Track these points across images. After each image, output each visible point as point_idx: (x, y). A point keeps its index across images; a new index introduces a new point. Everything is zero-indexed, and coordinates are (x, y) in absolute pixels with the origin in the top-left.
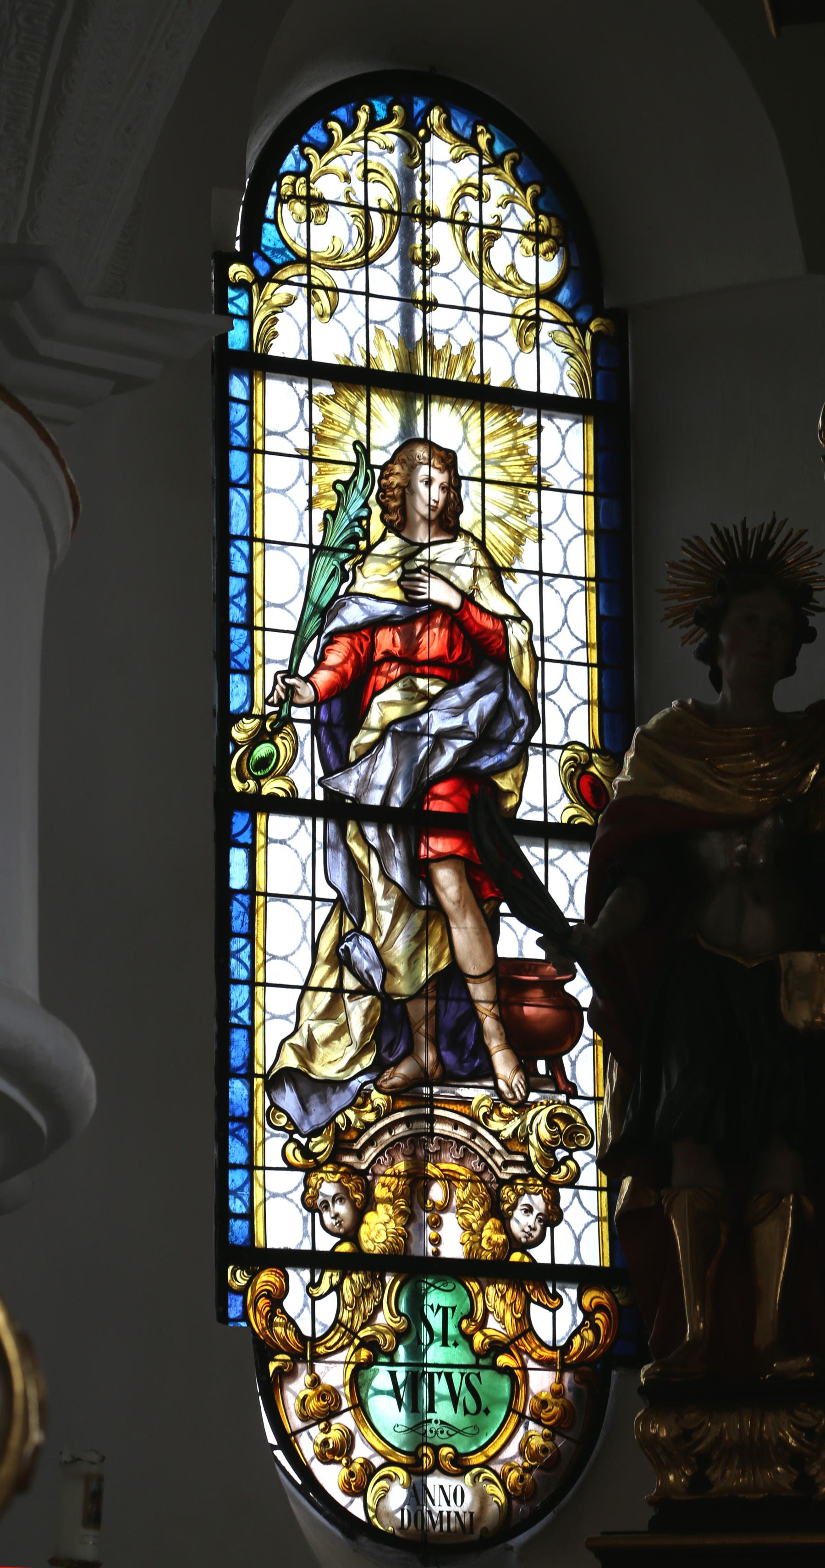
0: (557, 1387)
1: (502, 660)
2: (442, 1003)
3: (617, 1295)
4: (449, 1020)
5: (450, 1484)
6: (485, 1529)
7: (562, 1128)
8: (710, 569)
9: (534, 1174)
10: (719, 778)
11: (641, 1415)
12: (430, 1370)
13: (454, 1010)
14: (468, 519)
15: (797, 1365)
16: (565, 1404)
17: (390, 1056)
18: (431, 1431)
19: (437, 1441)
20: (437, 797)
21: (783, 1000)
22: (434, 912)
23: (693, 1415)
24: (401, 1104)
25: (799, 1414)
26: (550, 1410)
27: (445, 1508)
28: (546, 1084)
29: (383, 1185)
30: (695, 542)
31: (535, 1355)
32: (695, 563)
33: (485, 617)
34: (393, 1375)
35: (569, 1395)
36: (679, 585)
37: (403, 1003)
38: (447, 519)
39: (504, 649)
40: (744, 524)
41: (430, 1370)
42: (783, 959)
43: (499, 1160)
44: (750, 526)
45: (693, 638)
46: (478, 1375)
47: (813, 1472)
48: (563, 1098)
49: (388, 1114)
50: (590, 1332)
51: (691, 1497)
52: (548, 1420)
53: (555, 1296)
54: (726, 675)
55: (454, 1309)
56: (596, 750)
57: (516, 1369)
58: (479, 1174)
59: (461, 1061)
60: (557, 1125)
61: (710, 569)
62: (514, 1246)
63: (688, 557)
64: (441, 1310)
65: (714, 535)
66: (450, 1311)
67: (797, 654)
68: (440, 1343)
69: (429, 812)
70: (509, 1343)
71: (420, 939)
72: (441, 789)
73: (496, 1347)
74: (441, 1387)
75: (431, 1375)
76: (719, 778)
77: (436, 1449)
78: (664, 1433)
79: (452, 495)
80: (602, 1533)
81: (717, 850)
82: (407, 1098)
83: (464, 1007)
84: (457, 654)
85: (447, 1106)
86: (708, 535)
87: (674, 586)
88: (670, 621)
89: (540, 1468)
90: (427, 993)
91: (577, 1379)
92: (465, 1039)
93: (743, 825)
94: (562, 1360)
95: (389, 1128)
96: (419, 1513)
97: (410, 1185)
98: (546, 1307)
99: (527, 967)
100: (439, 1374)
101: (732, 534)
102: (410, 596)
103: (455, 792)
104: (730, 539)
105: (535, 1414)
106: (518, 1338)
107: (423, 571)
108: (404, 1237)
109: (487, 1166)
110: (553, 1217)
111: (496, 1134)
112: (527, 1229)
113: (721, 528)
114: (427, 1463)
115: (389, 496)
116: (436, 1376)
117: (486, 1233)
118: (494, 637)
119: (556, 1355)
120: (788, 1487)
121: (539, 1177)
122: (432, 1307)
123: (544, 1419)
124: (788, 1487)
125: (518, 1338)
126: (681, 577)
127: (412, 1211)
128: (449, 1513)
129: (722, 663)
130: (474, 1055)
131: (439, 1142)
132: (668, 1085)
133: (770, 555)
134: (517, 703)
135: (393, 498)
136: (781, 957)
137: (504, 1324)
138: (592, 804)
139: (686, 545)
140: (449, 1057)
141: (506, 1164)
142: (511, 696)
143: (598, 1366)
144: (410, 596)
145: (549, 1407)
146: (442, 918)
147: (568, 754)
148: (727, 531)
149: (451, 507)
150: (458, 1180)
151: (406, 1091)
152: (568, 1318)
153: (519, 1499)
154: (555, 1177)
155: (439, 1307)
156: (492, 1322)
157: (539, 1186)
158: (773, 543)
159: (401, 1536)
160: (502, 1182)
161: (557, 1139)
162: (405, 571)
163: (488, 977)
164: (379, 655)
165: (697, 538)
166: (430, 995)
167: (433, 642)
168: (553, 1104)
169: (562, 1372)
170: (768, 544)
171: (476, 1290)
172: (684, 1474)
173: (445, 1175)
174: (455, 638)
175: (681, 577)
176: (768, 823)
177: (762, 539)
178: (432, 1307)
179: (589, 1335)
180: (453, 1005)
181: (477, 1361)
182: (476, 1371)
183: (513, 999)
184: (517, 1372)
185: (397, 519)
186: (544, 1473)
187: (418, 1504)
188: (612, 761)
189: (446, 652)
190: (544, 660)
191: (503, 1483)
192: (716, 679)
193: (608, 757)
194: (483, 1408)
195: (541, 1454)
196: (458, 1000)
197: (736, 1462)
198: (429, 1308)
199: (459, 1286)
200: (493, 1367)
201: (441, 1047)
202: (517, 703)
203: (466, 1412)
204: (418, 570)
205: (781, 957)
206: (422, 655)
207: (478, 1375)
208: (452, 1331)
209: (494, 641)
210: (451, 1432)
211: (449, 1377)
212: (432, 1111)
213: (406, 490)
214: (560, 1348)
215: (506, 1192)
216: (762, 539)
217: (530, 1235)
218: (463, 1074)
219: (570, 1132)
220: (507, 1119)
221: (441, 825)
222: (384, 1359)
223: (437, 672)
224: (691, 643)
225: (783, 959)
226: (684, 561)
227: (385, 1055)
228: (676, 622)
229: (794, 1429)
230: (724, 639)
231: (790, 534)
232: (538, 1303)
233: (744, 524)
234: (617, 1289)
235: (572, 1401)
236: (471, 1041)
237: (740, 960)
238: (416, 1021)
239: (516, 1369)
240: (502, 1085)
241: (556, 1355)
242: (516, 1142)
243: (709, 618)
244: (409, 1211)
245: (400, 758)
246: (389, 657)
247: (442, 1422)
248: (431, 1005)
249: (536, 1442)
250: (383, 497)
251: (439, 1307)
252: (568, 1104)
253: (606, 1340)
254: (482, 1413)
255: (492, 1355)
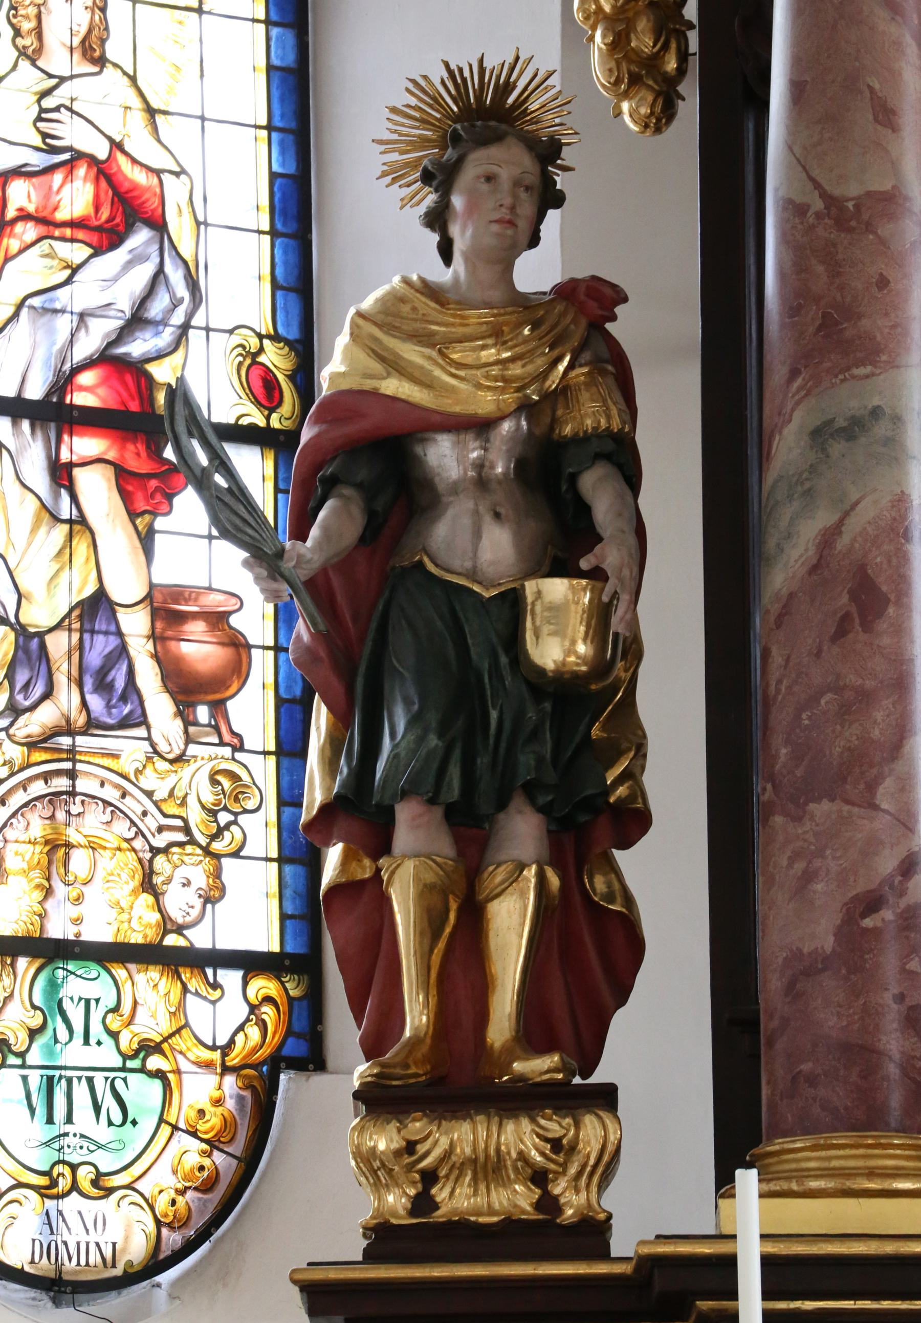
0: (217, 1094)
1: (159, 225)
2: (87, 636)
3: (287, 985)
4: (94, 659)
5: (91, 1208)
6: (130, 1263)
7: (226, 788)
8: (438, 116)
9: (193, 842)
10: (453, 370)
11: (357, 1124)
12: (69, 1073)
13: (100, 648)
14: (116, 49)
15: (539, 1066)
16: (226, 1114)
17: (25, 700)
18: (69, 1146)
19: (74, 1159)
20: (82, 388)
21: (529, 636)
22: (77, 527)
23: (418, 1124)
24: (37, 756)
25: (543, 1122)
26: (208, 1121)
27: (83, 1238)
28: (207, 734)
29: (16, 854)
30: (423, 83)
31: (189, 1055)
32: (420, 108)
33: (137, 169)
34: (25, 1078)
35: (230, 1104)
36: (400, 135)
37: (41, 635)
38: (91, 47)
39: (160, 210)
40: (481, 61)
41: (69, 1073)
42: (530, 587)
43: (154, 826)
44: (488, 65)
45: (413, 201)
46: (125, 1080)
47: (557, 1191)
48: (227, 751)
49: (22, 769)
50: (256, 1028)
51: (414, 1221)
52: (206, 1133)
53: (215, 986)
54: (459, 247)
55: (97, 1001)
56: (269, 337)
57: (170, 1072)
58: (128, 841)
59: (109, 706)
60: (219, 783)
61: (438, 116)
62: (169, 927)
63: (413, 101)
64: (83, 1001)
65: (445, 75)
66: (93, 1003)
67: (541, 223)
68: (82, 1041)
69: (72, 406)
70: (162, 1042)
71: (67, 550)
72: (87, 378)
73: (148, 1048)
74: (81, 1092)
75: (69, 1081)
76: (453, 370)
77: (74, 1168)
78: (382, 1146)
79: (97, 18)
80: (309, 1264)
81: (445, 457)
82: (46, 749)
83: (113, 642)
84: (105, 214)
85: (92, 760)
86: (438, 74)
87: (395, 137)
88: (388, 179)
89: (196, 1189)
90: (70, 624)
91: (240, 1084)
92: (113, 680)
93: (482, 427)
94: (223, 1062)
95: (24, 785)
96: (53, 1244)
97: (48, 853)
98: (205, 998)
99: (187, 595)
100: (79, 1079)
101: (467, 74)
102: (48, 141)
103: (104, 381)
104: (464, 80)
105: (190, 1126)
106: (172, 1035)
107: (62, 109)
108: (40, 915)
109: (140, 833)
110: (213, 896)
111: (149, 794)
112: (186, 908)
113: (453, 66)
114: (64, 1184)
115: (22, 16)
116: (75, 1081)
117: (135, 913)
118: (146, 196)
119: (216, 1056)
120: (528, 1208)
121: (200, 846)
122: (72, 999)
123: (200, 1132)
124: (528, 1208)
125: (172, 1035)
126: (403, 125)
127: (50, 885)
128: (88, 1244)
129: (455, 230)
130: (124, 698)
131: (83, 802)
132: (393, 735)
133: (510, 101)
134: (175, 275)
135: (27, 17)
136: (527, 584)
137: (156, 1019)
138: (263, 402)
139: (411, 86)
140: (96, 703)
141: (160, 829)
142: (169, 268)
143: (265, 1069)
144: (48, 141)
145: (207, 1117)
146: (88, 534)
147: (236, 339)
148: (461, 70)
149: (96, 32)
150: (105, 848)
151: (45, 740)
152: (233, 1009)
153: (170, 1226)
154: (216, 846)
155: (80, 999)
156: (142, 1015)
157: (198, 855)
158: (514, 87)
159: (32, 1271)
160: (155, 851)
161: (220, 800)
162: (42, 110)
163: (141, 606)
164: (11, 213)
165: (425, 77)
166: (73, 626)
167: (77, 197)
168: (216, 758)
169: (222, 1075)
170: (506, 88)
171: (123, 979)
172: (405, 1192)
173: (89, 842)
174: (102, 195)
175: (403, 125)
176: (506, 426)
177: (501, 81)
178: (72, 999)
179: (254, 1033)
180: (100, 639)
181: (124, 1063)
182: (123, 1075)
183: (169, 633)
184: (171, 1076)
185: (32, 44)
186: (200, 1195)
187: (52, 1233)
188: (287, 349)
189: (91, 211)
190: (206, 224)
191: (152, 1208)
192: (446, 251)
193: (282, 345)
194: (130, 1119)
195: (197, 1174)
196: (106, 633)
197: (468, 1179)
198: (69, 1000)
199: (104, 973)
200: (142, 1070)
201: (86, 690)
202: (175, 275)
203: (110, 1123)
204: (57, 109)
205: (527, 584)
206: (62, 215)
207: (125, 1080)
208: (96, 1030)
209: (147, 200)
210: (92, 1147)
211: (90, 1081)
212: (74, 766)
213: (42, 9)
214: (220, 1047)
215: (160, 862)
216: (501, 81)
217: (188, 913)
218: (111, 721)
219: (233, 791)
220: (162, 776)
221: (90, 420)
222: (12, 1060)
223: (80, 235)
224: (411, 207)
225: (530, 587)
226: (408, 106)
227: (19, 698)
228: (394, 180)
229: (537, 1140)
230: (457, 201)
231: (536, 75)
232: (197, 994)
233: (481, 61)
234: (287, 979)
235: (233, 1111)
236: (120, 684)
237: (476, 588)
238: (56, 658)
239: (170, 1072)
240: (156, 737)
241: (216, 1056)
242: (173, 803)
243: (441, 177)
244: (47, 885)
245: (38, 339)
246: (24, 216)
247: (82, 1136)
248: (76, 637)
249: (193, 1160)
250: (15, 16)
251: (80, 999)
252: (233, 759)
253: (273, 1037)
254: (128, 1124)
255: (142, 1055)
